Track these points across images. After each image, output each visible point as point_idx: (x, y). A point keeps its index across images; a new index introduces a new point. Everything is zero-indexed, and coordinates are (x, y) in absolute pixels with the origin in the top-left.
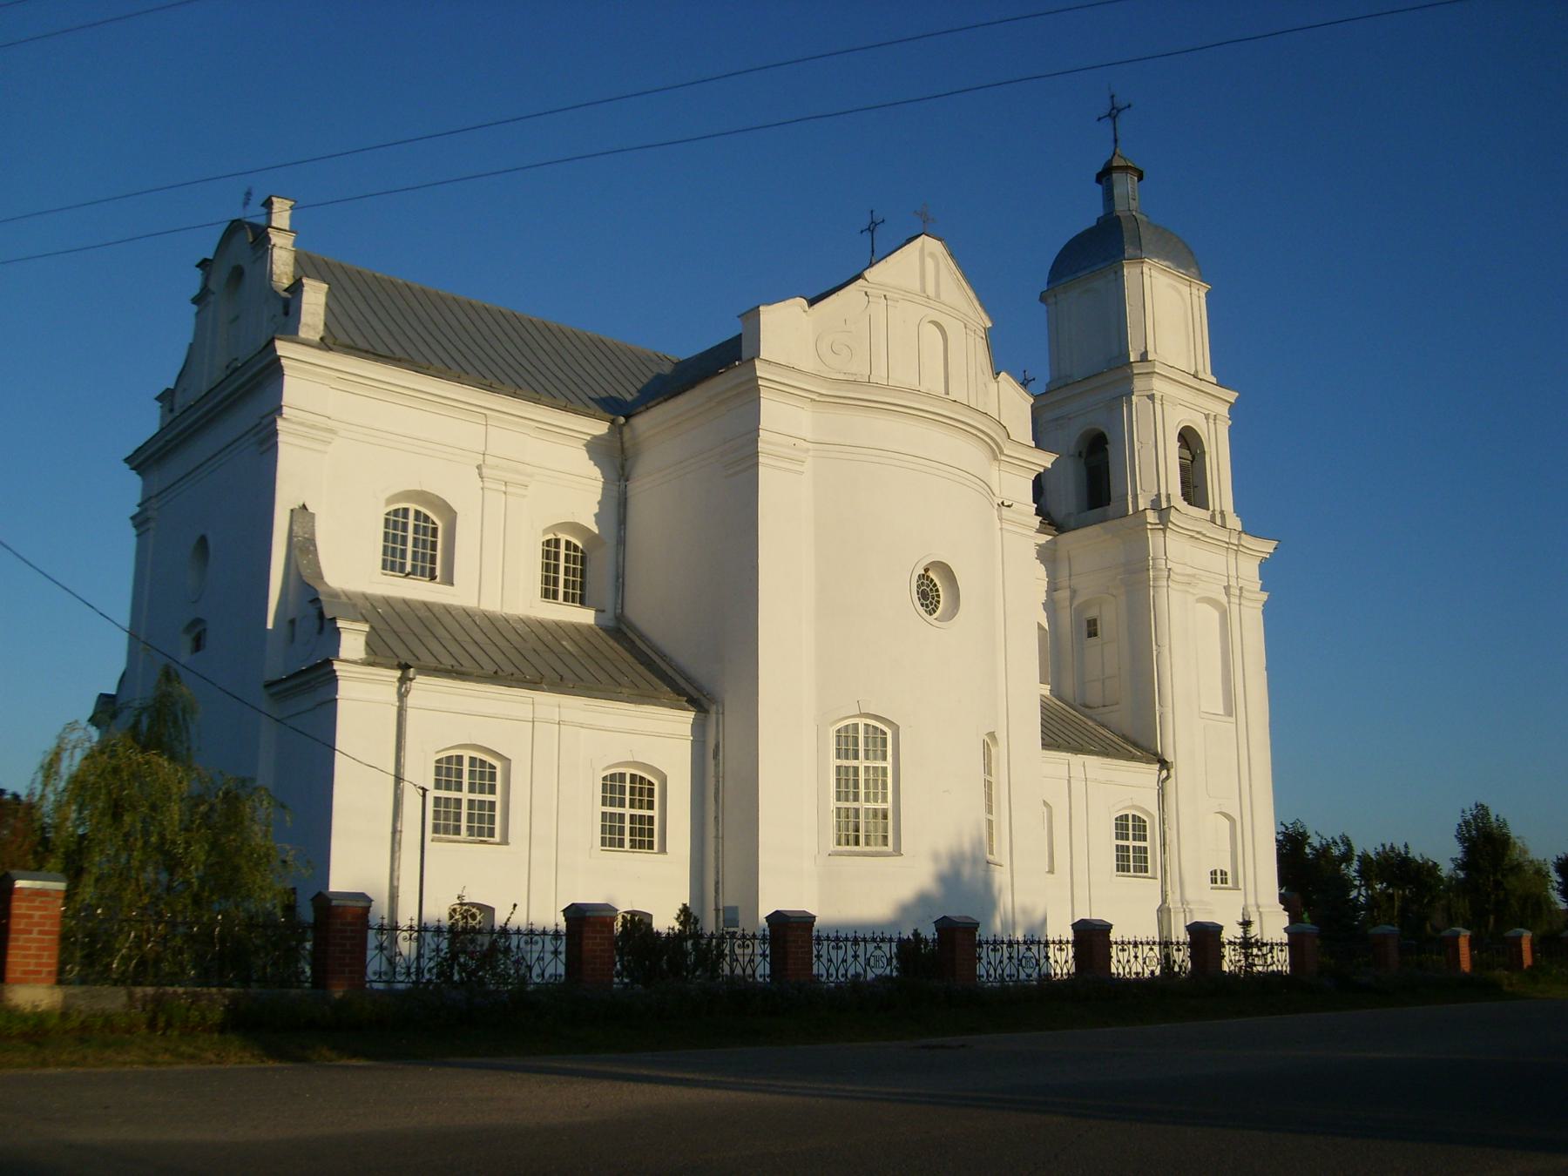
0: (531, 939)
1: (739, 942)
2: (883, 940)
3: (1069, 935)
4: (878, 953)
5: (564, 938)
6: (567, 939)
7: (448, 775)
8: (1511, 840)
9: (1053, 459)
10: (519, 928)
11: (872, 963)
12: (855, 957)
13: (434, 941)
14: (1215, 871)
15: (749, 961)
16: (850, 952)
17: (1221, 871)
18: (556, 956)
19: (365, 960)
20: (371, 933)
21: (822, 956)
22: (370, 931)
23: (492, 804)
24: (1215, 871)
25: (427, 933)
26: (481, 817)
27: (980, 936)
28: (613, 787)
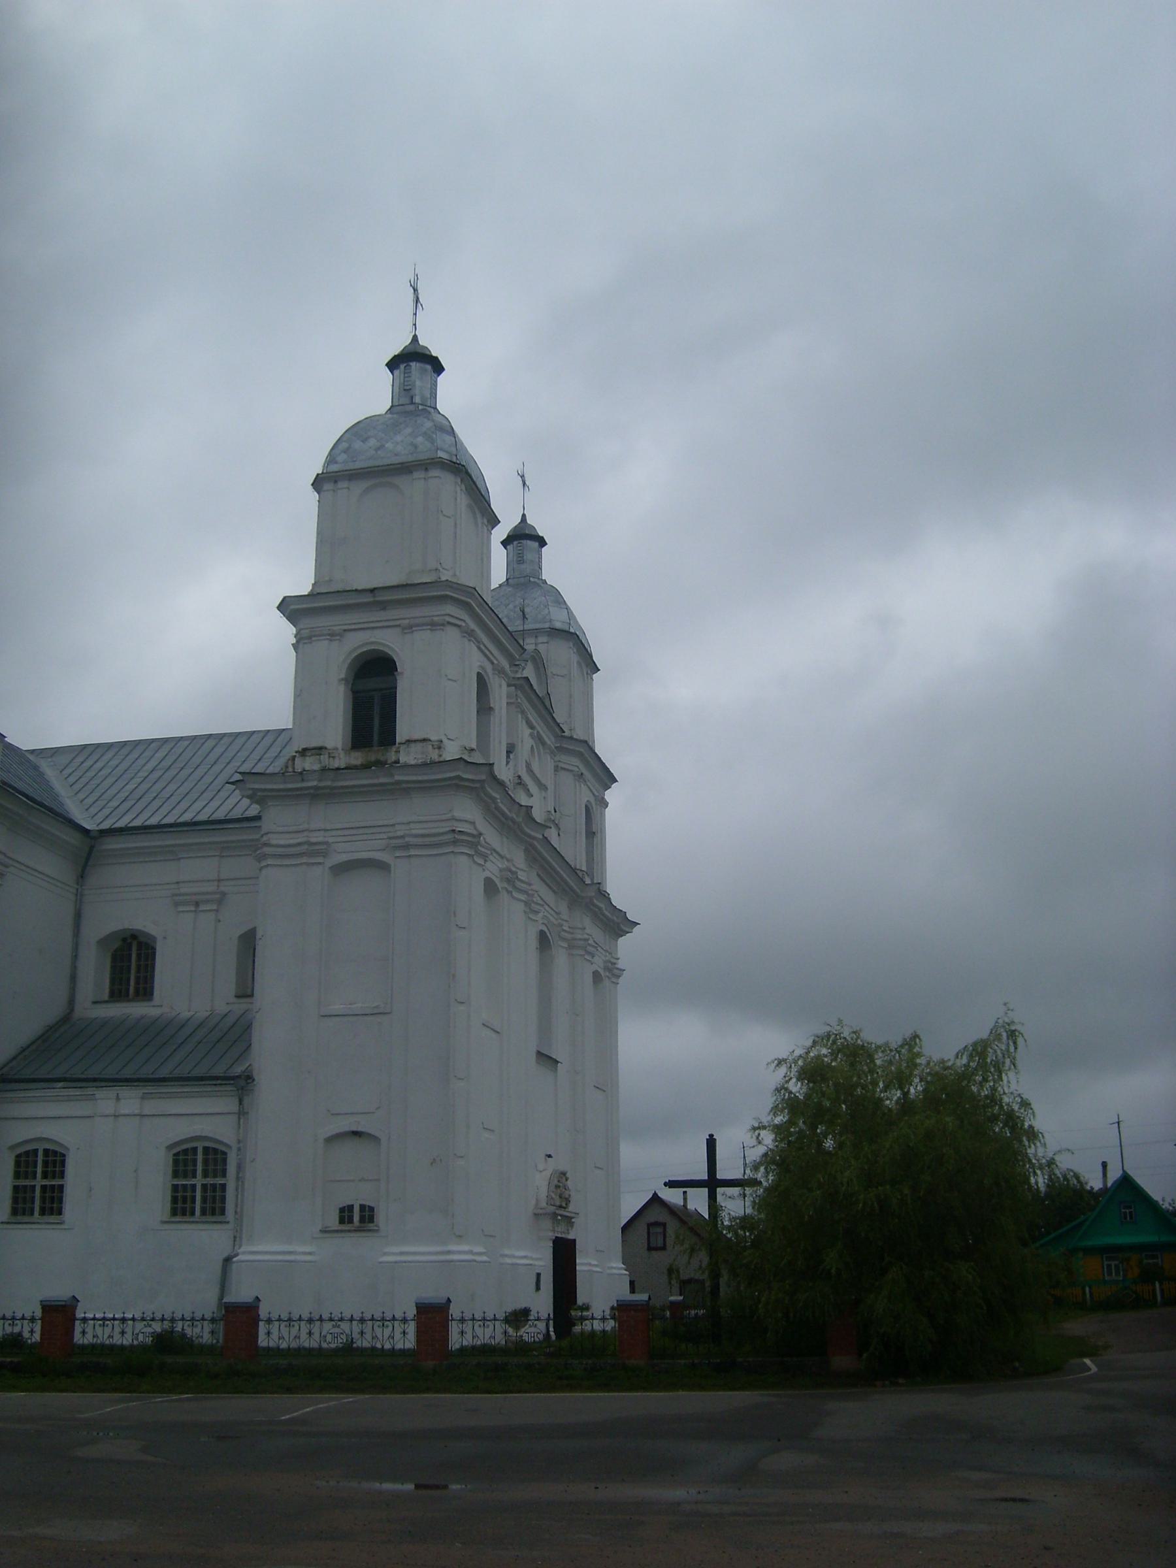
0: (13, 1322)
1: (188, 1322)
2: (341, 1319)
3: (412, 1312)
4: (337, 1330)
5: (39, 1322)
6: (554, 1323)
7: (214, 1198)
8: (364, 763)
9: (492, 586)
10: (4, 1315)
11: (329, 1338)
12: (310, 1334)
13: (307, 1327)
14: (351, 1208)
15: (295, 1337)
16: (117, 1330)
17: (362, 1207)
18: (310, 1336)
19: (258, 1341)
20: (261, 1324)
21: (313, 1334)
22: (76, 1321)
23: (223, 1187)
24: (351, 1208)
25: (594, 1321)
26: (52, 1202)
27: (452, 1315)
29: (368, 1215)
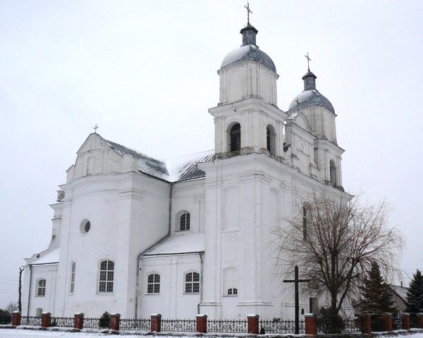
3: (73, 317)
17: (234, 289)
28: (188, 277)
29: (235, 291)
